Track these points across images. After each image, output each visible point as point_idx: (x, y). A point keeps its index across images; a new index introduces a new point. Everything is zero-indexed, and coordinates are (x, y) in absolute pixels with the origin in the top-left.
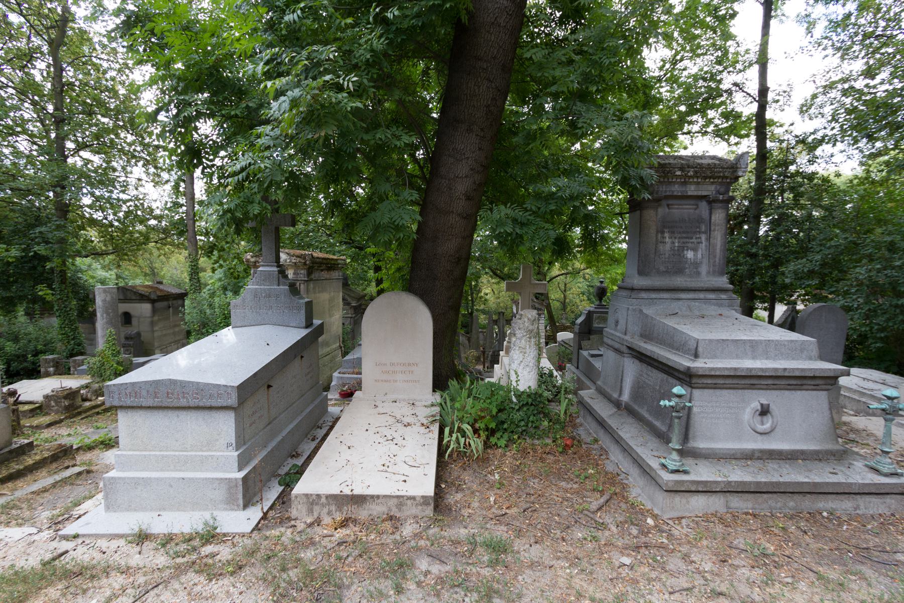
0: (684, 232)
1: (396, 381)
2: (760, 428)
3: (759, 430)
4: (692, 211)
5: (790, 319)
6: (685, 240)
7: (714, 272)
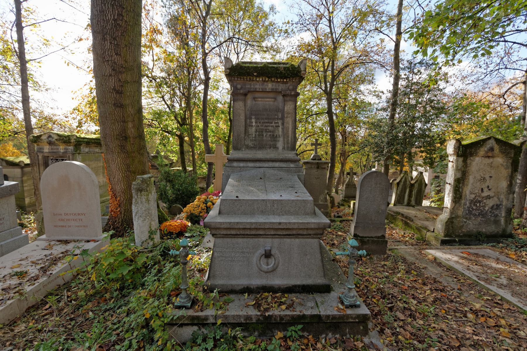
0: (266, 119)
1: (70, 226)
2: (265, 267)
3: (270, 270)
4: (271, 103)
5: (403, 179)
6: (267, 124)
7: (288, 148)
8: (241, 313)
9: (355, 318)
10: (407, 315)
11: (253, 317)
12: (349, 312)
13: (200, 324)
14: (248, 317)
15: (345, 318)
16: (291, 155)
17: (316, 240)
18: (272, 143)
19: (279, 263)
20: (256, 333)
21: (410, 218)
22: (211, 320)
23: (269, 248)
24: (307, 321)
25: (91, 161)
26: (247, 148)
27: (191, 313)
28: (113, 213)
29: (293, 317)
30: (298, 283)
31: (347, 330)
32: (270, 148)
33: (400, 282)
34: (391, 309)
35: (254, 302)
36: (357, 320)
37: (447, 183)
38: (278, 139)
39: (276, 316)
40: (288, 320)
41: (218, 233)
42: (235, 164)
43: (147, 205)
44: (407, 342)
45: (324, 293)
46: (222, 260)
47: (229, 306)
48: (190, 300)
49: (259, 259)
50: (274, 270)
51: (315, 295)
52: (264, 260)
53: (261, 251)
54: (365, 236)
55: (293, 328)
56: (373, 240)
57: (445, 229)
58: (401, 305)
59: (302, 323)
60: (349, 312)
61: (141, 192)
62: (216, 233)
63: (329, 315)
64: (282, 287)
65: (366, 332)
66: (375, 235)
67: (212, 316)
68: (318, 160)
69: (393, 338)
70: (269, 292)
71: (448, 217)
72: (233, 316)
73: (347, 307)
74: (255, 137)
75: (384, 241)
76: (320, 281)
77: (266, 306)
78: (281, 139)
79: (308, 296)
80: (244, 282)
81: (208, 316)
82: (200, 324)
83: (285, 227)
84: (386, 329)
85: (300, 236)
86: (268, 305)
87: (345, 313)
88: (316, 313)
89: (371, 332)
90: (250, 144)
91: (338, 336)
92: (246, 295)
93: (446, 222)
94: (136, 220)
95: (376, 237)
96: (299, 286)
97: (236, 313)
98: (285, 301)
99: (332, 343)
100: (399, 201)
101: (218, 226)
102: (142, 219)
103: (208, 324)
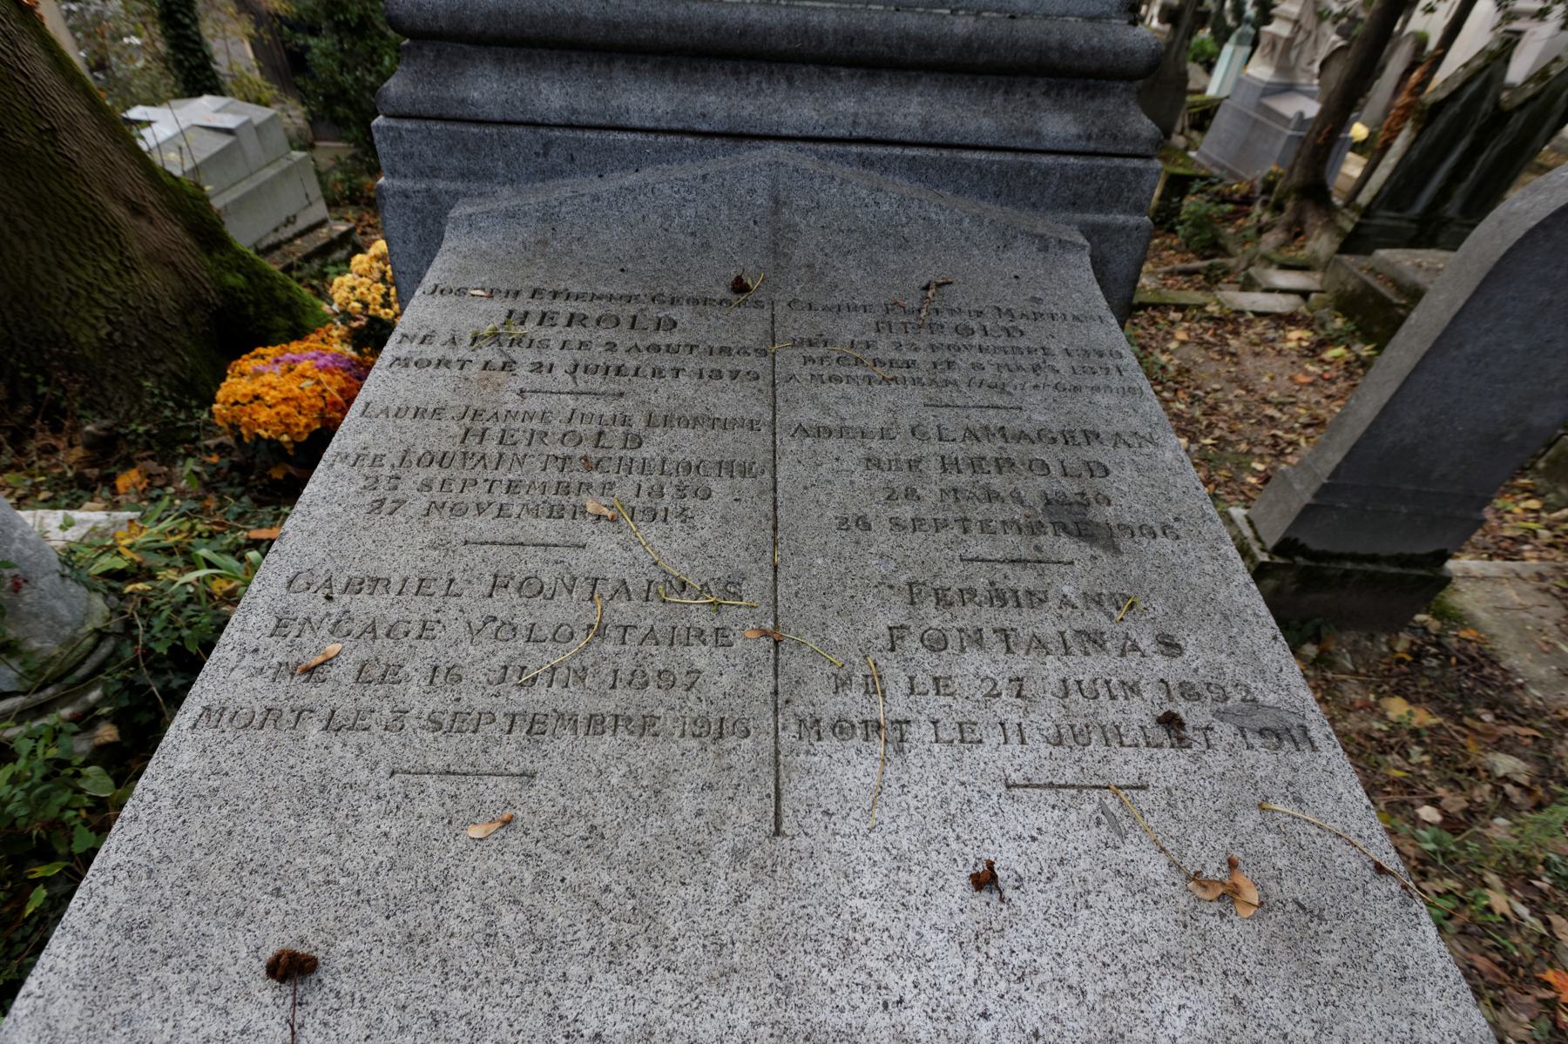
54: (1337, 550)
95: (1399, 560)
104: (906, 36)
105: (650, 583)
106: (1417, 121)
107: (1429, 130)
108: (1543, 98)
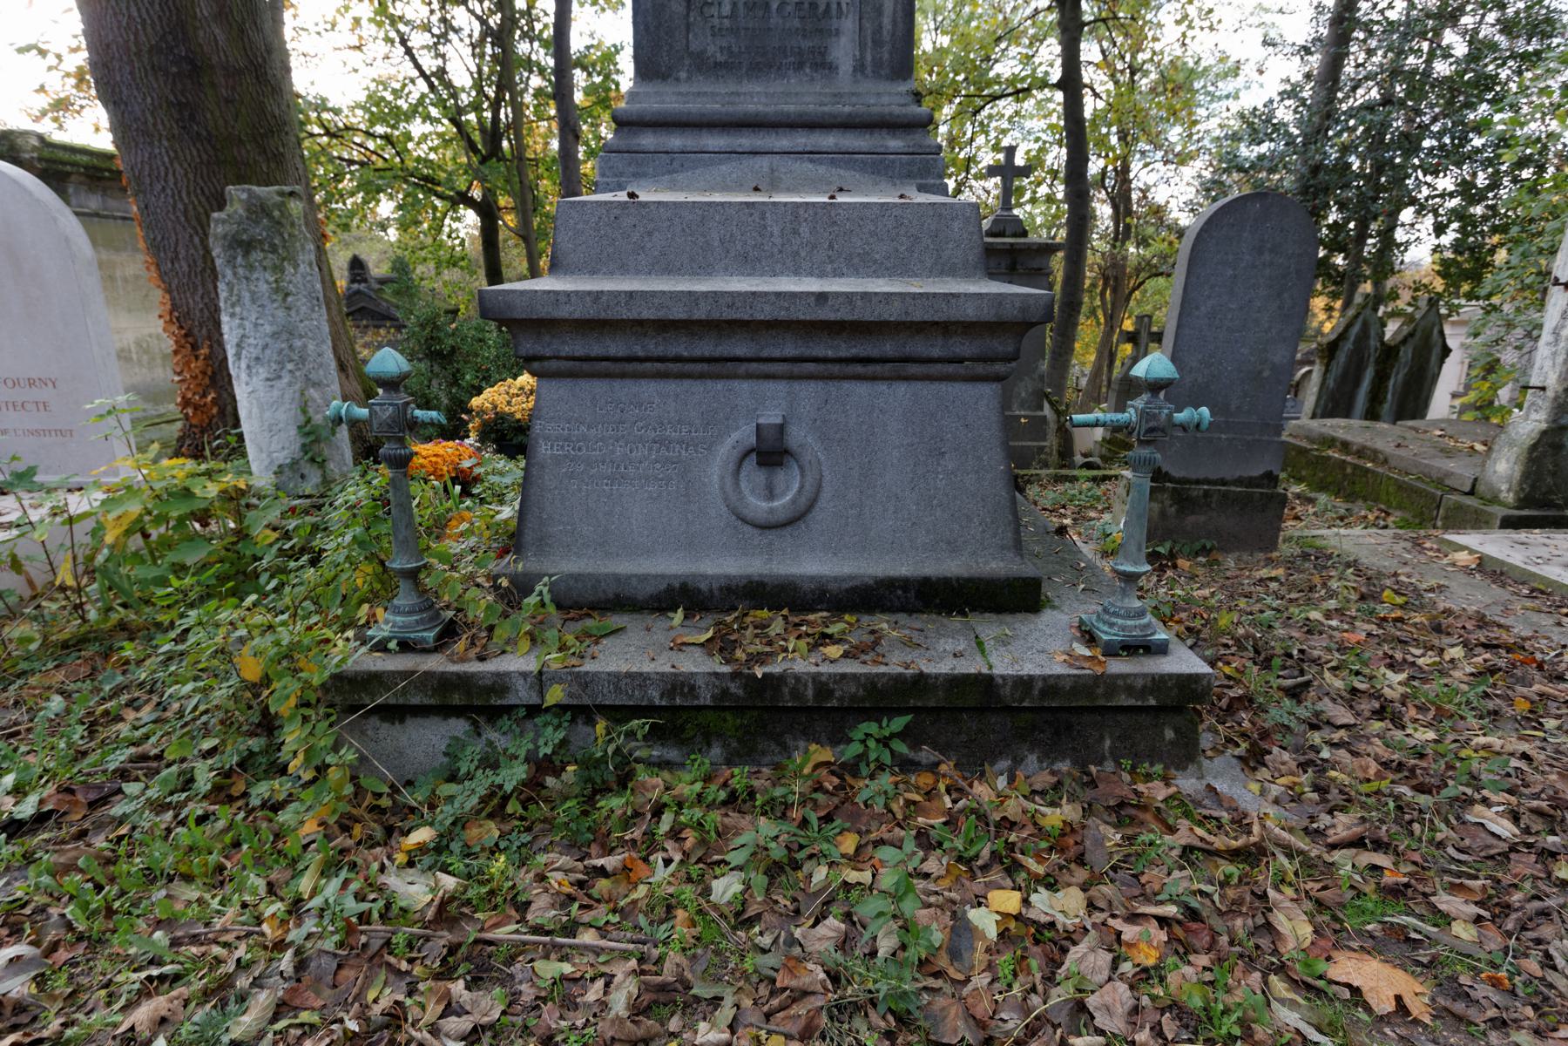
2: (758, 506)
3: (782, 516)
7: (878, 64)
8: (648, 668)
9: (1143, 692)
10: (1367, 714)
11: (700, 682)
12: (1118, 666)
13: (480, 710)
14: (678, 684)
15: (1100, 691)
16: (888, 98)
17: (988, 391)
18: (806, 44)
19: (819, 487)
20: (716, 751)
21: (1376, 451)
22: (523, 694)
23: (779, 421)
24: (932, 704)
25: (117, 250)
26: (699, 69)
27: (435, 663)
28: (190, 411)
29: (871, 683)
30: (904, 568)
31: (1108, 743)
32: (799, 66)
33: (1334, 623)
34: (1296, 693)
35: (710, 634)
36: (1152, 702)
37: (1557, 282)
38: (835, 23)
39: (797, 678)
40: (853, 698)
41: (548, 352)
42: (648, 140)
43: (281, 313)
44: (1365, 788)
45: (1013, 610)
46: (571, 476)
47: (600, 647)
48: (431, 619)
49: (732, 467)
50: (795, 519)
51: (975, 619)
52: (753, 475)
53: (744, 434)
54: (1193, 476)
55: (872, 728)
56: (1225, 495)
57: (1526, 476)
58: (1339, 684)
59: (914, 710)
60: (1118, 666)
61: (246, 254)
62: (538, 349)
63: (1031, 678)
64: (832, 586)
65: (1186, 754)
66: (1237, 474)
67: (524, 675)
68: (1014, 235)
69: (1305, 778)
70: (775, 607)
71: (1544, 426)
72: (616, 678)
73: (1111, 651)
74: (733, 15)
75: (1271, 497)
76: (996, 565)
77: (758, 647)
78: (849, 24)
79: (945, 621)
80: (670, 566)
81: (507, 674)
82: (480, 710)
83: (844, 314)
84: (1275, 750)
85: (913, 369)
86: (770, 643)
87: (1099, 670)
88: (973, 671)
89: (1211, 758)
90: (711, 49)
91: (1064, 766)
92: (680, 612)
93: (1534, 447)
94: (244, 376)
95: (1239, 481)
96: (904, 584)
97: (624, 668)
98: (843, 632)
99: (1038, 787)
100: (1335, 404)
101: (544, 312)
102: (263, 372)
103: (509, 709)
104: (824, 113)
105: (768, 1016)
106: (1322, 358)
107: (1334, 363)
108: (1418, 335)
